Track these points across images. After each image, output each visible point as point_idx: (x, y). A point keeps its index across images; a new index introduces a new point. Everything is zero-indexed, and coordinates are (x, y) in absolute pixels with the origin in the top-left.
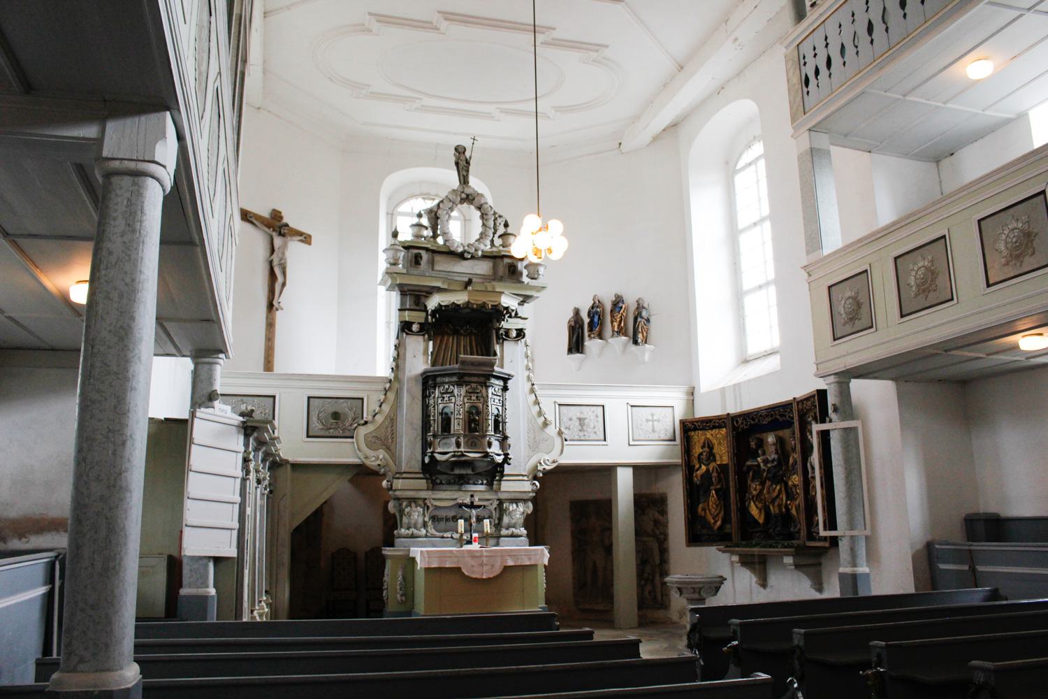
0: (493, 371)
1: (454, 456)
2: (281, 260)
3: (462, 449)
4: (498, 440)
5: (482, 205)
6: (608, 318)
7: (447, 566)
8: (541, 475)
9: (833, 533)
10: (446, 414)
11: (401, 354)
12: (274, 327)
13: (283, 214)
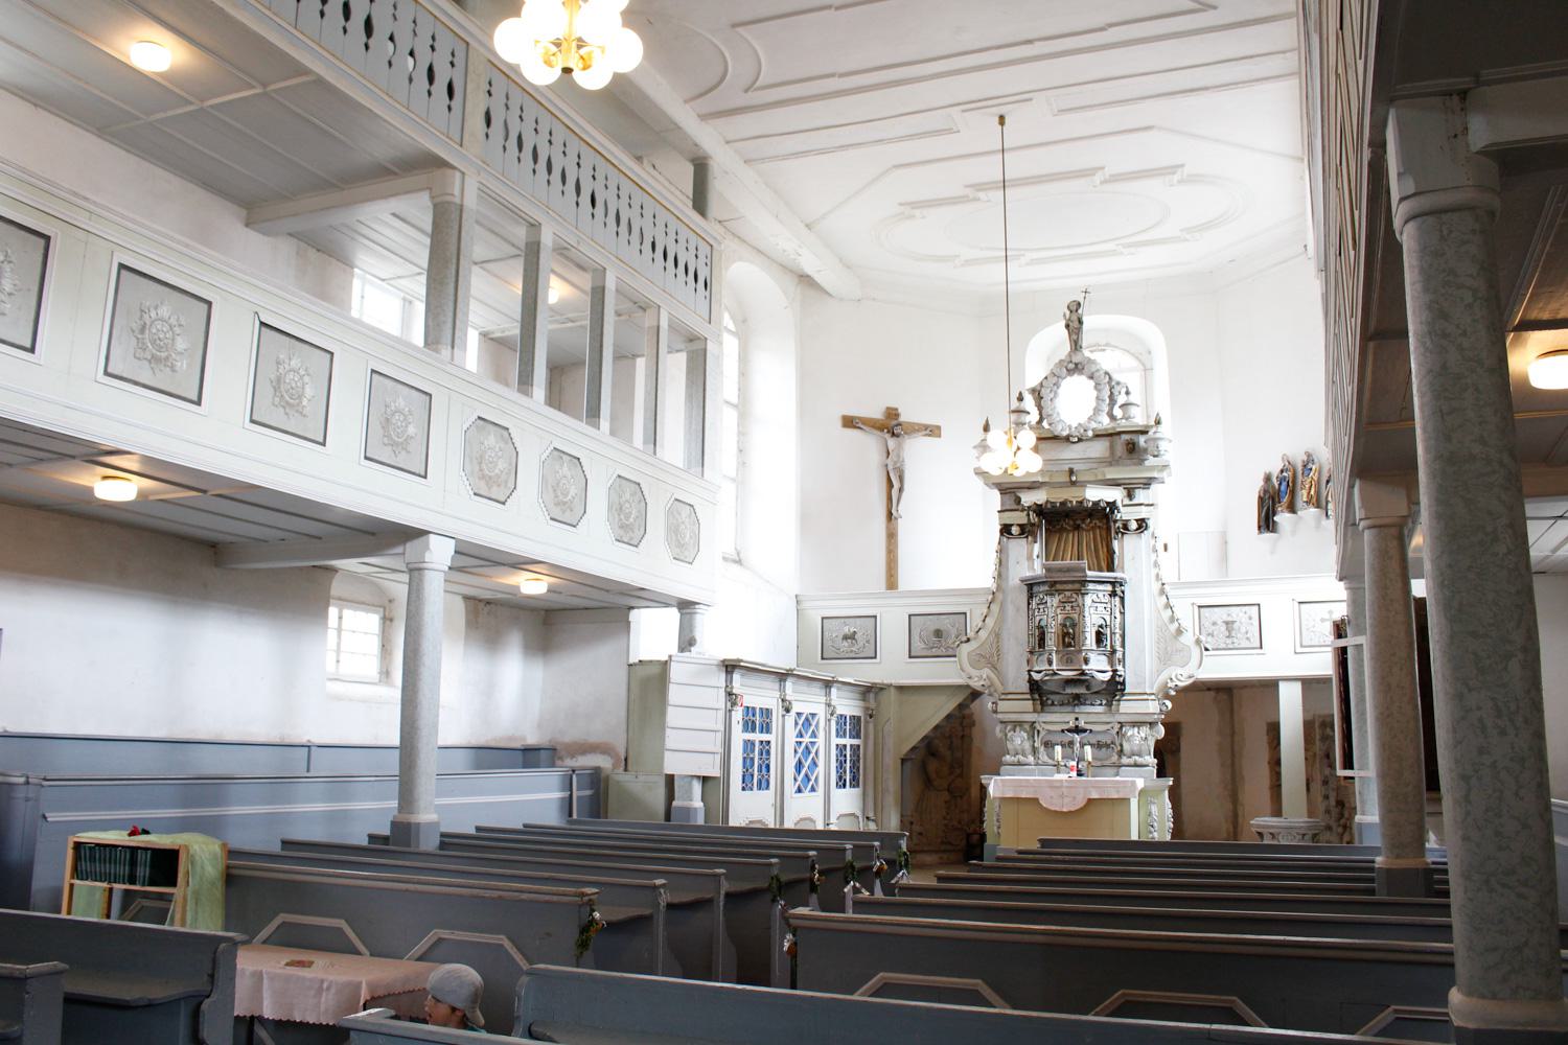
0: (1086, 576)
1: (1047, 675)
2: (895, 463)
3: (1054, 667)
5: (1093, 374)
7: (1023, 796)
8: (1173, 693)
9: (1348, 773)
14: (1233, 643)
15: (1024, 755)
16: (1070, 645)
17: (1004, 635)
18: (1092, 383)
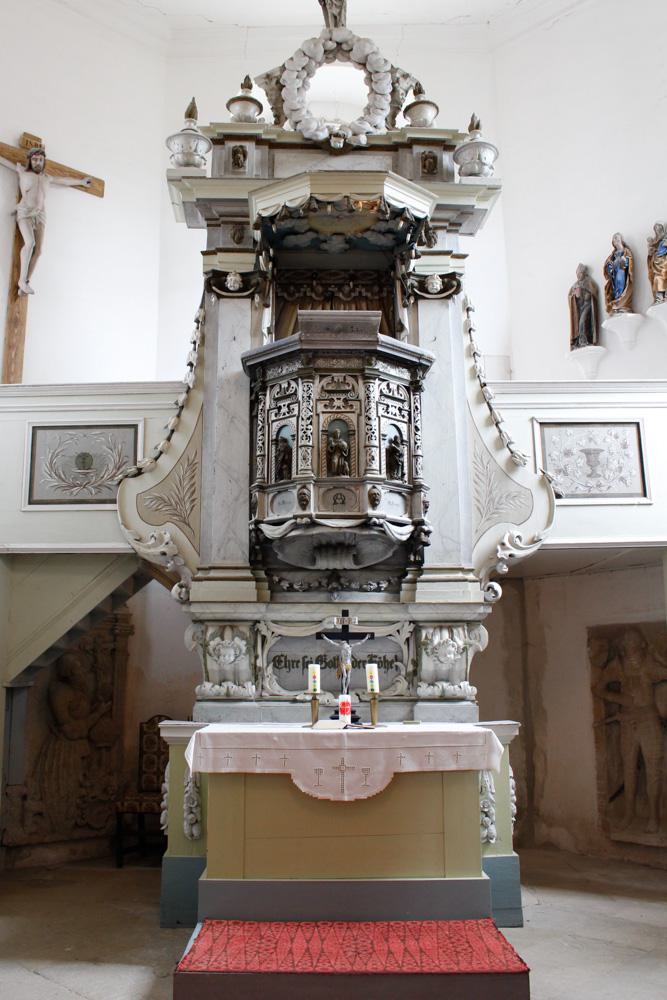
1: (296, 526)
2: (30, 210)
3: (312, 510)
4: (400, 493)
5: (366, 57)
6: (644, 271)
7: (258, 771)
8: (505, 569)
10: (285, 440)
11: (208, 336)
12: (23, 324)
13: (43, 143)
14: (599, 486)
15: (238, 682)
16: (341, 471)
17: (207, 463)
18: (362, 74)
